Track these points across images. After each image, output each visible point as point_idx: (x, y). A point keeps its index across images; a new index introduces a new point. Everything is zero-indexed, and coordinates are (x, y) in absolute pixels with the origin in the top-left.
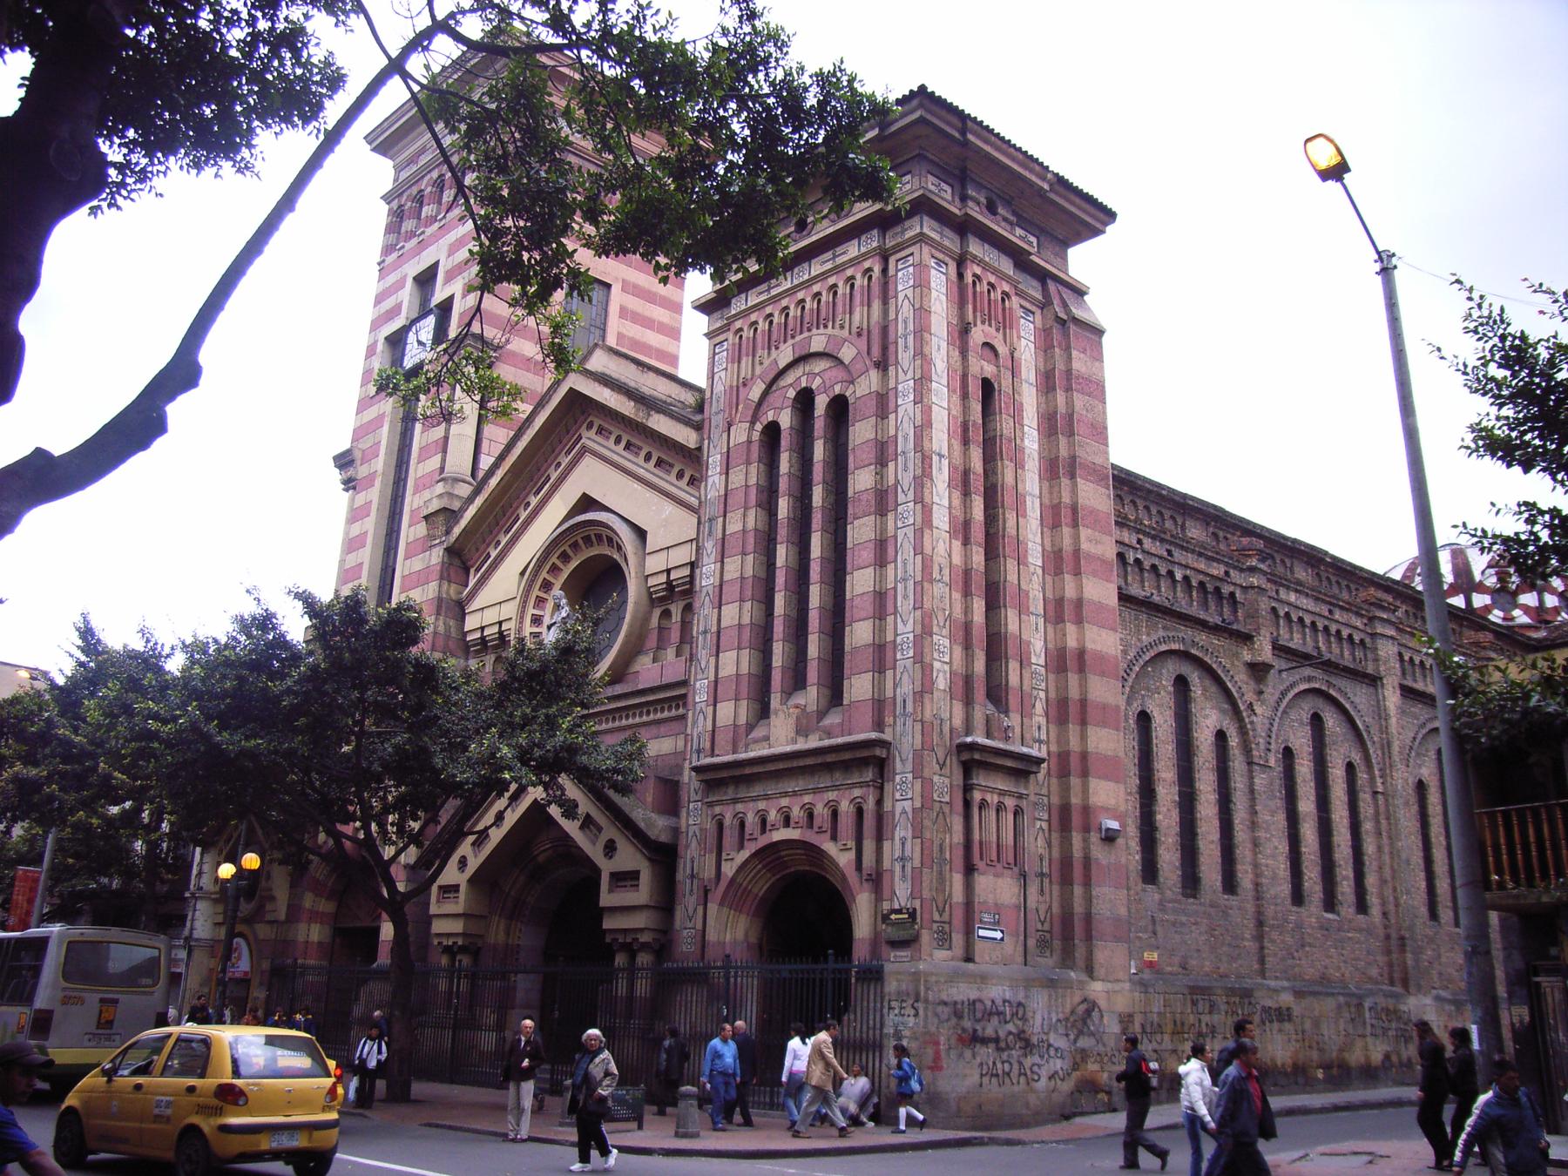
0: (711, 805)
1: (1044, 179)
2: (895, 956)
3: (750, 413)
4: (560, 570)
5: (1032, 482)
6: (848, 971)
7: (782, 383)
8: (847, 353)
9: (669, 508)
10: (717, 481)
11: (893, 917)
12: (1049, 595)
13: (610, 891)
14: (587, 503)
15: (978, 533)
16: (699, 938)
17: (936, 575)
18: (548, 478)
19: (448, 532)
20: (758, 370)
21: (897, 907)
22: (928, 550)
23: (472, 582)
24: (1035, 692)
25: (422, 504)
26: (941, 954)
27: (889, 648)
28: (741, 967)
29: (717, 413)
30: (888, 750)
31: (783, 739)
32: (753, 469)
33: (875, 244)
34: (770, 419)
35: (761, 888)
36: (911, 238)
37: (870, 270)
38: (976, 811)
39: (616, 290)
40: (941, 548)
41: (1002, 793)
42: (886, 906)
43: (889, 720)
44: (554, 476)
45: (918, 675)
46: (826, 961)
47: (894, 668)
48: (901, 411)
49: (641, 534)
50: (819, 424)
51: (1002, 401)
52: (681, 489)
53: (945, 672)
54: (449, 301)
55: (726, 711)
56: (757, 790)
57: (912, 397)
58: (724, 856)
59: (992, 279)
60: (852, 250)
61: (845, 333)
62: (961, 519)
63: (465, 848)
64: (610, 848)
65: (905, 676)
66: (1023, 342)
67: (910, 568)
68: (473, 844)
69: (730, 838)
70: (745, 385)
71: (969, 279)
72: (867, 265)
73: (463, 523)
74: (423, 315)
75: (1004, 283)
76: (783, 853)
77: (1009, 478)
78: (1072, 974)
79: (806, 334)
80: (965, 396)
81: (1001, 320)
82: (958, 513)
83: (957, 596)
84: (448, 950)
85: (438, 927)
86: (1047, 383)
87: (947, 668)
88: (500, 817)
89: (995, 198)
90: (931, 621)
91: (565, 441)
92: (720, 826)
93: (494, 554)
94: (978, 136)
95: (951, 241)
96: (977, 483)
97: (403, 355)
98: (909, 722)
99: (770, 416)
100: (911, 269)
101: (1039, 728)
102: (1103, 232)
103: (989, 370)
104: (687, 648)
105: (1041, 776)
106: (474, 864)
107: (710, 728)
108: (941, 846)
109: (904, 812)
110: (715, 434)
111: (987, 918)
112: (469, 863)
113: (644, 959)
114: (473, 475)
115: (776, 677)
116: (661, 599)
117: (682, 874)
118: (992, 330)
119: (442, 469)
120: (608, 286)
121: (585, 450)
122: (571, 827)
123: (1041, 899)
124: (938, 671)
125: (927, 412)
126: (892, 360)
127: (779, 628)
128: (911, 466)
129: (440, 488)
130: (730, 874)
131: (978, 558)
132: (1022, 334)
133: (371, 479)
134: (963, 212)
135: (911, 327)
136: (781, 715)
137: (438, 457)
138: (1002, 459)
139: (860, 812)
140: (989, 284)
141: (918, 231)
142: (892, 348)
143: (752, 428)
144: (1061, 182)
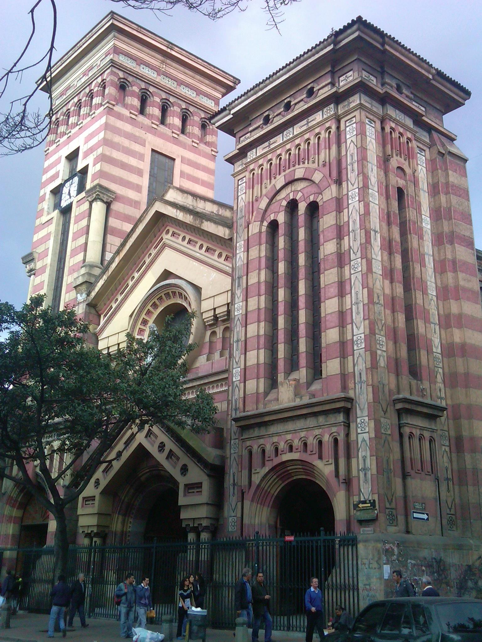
0: (244, 440)
1: (429, 72)
2: (363, 531)
3: (260, 216)
4: (152, 313)
5: (428, 247)
6: (333, 541)
7: (278, 197)
8: (317, 177)
9: (215, 274)
10: (242, 256)
11: (361, 505)
12: (441, 312)
13: (185, 495)
14: (166, 274)
15: (399, 276)
16: (240, 522)
17: (376, 300)
18: (145, 262)
19: (88, 295)
20: (264, 192)
21: (362, 499)
22: (371, 285)
23: (102, 322)
24: (436, 369)
25: (73, 280)
26: (392, 529)
27: (349, 343)
28: (264, 540)
29: (241, 218)
30: (352, 403)
31: (286, 400)
32: (263, 247)
33: (332, 113)
34: (272, 219)
35: (275, 491)
36: (354, 107)
37: (329, 128)
38: (406, 440)
39: (178, 162)
40: (378, 285)
41: (422, 429)
42: (356, 499)
43: (351, 385)
44: (148, 261)
45: (369, 358)
46: (319, 534)
47: (353, 355)
48: (351, 207)
49: (198, 289)
51: (408, 201)
52: (221, 263)
53: (384, 357)
54: (86, 168)
55: (251, 385)
56: (273, 429)
57: (357, 198)
58: (253, 471)
59: (401, 130)
60: (318, 117)
61: (316, 165)
62: (389, 268)
63: (99, 474)
64: (184, 470)
65: (360, 360)
66: (420, 167)
67: (360, 296)
68: (103, 471)
69: (257, 460)
70: (257, 200)
71: (388, 130)
72: (327, 125)
73: (97, 289)
74: (71, 178)
75: (408, 133)
76: (289, 468)
77: (415, 244)
78: (471, 541)
79: (292, 169)
80: (388, 197)
81: (407, 153)
82: (387, 264)
83: (388, 312)
84: (88, 535)
85: (82, 521)
86: (434, 190)
87: (385, 354)
88: (119, 454)
89: (401, 84)
90: (375, 327)
91: (121, 576)
92: (250, 453)
93: (114, 306)
94: (392, 47)
95: (377, 108)
96: (397, 247)
97: (61, 200)
98: (364, 386)
99: (272, 217)
100: (354, 125)
101: (440, 390)
102: (464, 104)
103: (401, 183)
104: (227, 353)
105: (443, 419)
106: (103, 483)
107: (242, 395)
108: (387, 461)
109: (364, 440)
110: (240, 229)
111: (418, 506)
112: (101, 483)
113: (204, 536)
114: (102, 263)
115: (281, 364)
116: (210, 325)
117: (229, 481)
118: (402, 160)
119: (84, 260)
120: (174, 160)
121: (165, 246)
122: (161, 458)
123: (448, 494)
124: (380, 356)
125: (367, 206)
126: (344, 177)
127: (281, 336)
128: (358, 237)
129: (83, 271)
130: (257, 482)
131: (399, 290)
132: (419, 162)
133: (43, 269)
134: (384, 91)
135: (355, 158)
136: (285, 386)
137: (82, 254)
138: (410, 233)
139: (336, 441)
140: (400, 133)
141: (358, 102)
142: (344, 172)
143: (261, 225)
144: (440, 74)
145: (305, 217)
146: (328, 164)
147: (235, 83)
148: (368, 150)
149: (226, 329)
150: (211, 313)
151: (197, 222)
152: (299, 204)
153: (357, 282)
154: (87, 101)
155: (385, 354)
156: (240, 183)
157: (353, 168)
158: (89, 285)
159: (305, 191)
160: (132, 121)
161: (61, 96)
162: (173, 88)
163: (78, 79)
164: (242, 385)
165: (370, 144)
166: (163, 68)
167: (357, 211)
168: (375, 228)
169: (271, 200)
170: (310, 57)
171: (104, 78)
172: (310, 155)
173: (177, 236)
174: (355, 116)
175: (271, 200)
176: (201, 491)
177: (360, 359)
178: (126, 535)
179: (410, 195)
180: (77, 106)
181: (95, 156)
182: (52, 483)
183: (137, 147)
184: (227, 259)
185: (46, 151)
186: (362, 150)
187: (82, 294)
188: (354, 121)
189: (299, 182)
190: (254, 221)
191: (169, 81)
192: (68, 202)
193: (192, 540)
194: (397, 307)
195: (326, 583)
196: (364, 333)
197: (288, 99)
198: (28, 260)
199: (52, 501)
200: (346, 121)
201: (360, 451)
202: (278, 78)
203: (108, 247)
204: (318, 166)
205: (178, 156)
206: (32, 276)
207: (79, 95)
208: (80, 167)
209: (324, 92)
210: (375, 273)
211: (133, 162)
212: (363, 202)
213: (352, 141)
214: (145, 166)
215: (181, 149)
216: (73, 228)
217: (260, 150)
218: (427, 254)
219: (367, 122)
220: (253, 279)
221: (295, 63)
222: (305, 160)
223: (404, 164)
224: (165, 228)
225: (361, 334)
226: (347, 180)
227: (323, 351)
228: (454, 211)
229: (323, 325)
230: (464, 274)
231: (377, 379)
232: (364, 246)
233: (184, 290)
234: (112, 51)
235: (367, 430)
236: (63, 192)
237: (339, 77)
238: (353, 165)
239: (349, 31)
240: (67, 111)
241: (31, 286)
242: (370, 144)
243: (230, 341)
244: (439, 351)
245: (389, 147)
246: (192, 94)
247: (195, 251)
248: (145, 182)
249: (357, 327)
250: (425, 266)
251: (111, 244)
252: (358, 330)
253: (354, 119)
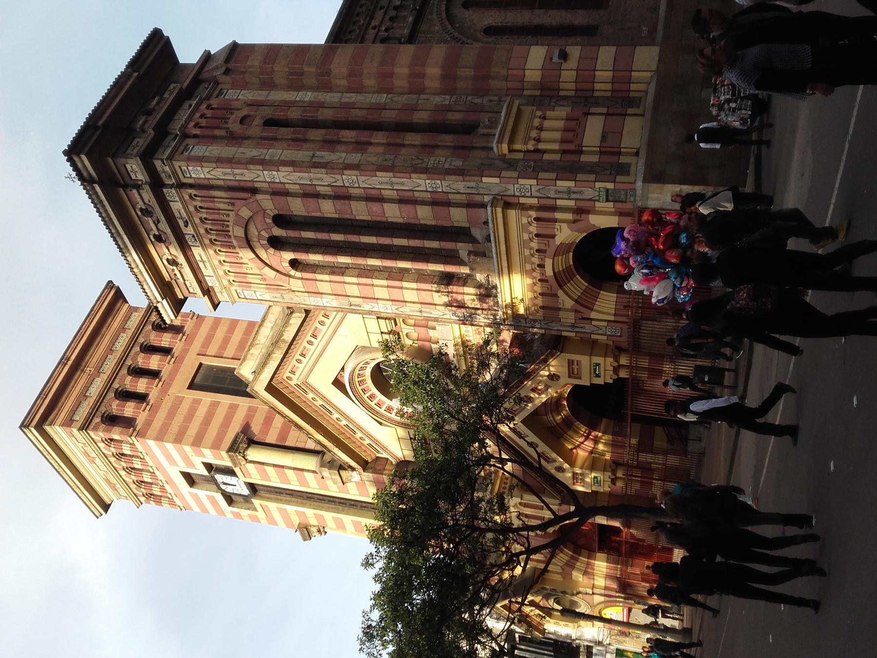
5: (333, 98)
8: (245, 213)
10: (327, 300)
11: (597, 373)
14: (338, 383)
15: (364, 136)
17: (390, 163)
19: (353, 469)
23: (385, 455)
37: (190, 196)
40: (373, 159)
50: (292, 234)
51: (279, 115)
53: (452, 161)
57: (275, 173)
59: (198, 115)
60: (176, 207)
70: (265, 280)
71: (197, 131)
72: (187, 197)
80: (275, 139)
84: (613, 481)
86: (268, 84)
93: (368, 441)
96: (331, 134)
100: (190, 168)
103: (258, 121)
104: (431, 323)
109: (539, 191)
118: (233, 117)
120: (201, 364)
124: (450, 165)
126: (249, 185)
131: (380, 137)
132: (235, 97)
133: (318, 517)
135: (229, 170)
138: (317, 117)
142: (242, 184)
145: (290, 229)
146: (232, 201)
147: (112, 288)
148: (220, 156)
151: (282, 345)
152: (274, 235)
153: (368, 182)
154: (127, 461)
155: (449, 160)
156: (243, 297)
157: (239, 175)
159: (260, 227)
160: (154, 410)
161: (116, 490)
162: (116, 360)
163: (98, 469)
165: (213, 152)
166: (90, 371)
167: (288, 174)
168: (309, 156)
169: (266, 264)
170: (106, 211)
172: (220, 219)
173: (295, 368)
174: (180, 167)
175: (266, 264)
176: (577, 361)
177: (452, 186)
178: (617, 442)
179: (273, 112)
180: (130, 472)
181: (193, 454)
182: (557, 519)
184: (326, 316)
185: (181, 510)
186: (220, 161)
189: (248, 232)
191: (107, 364)
192: (244, 487)
193: (627, 362)
194: (399, 141)
196: (425, 180)
197: (152, 237)
199: (576, 519)
200: (185, 177)
201: (549, 195)
203: (300, 445)
204: (232, 211)
205: (197, 358)
206: (326, 530)
207: (118, 470)
208: (205, 472)
209: (148, 195)
210: (360, 161)
211: (201, 412)
212: (280, 168)
213: (208, 172)
214: (207, 398)
215: (189, 355)
216: (275, 481)
218: (341, 99)
219: (187, 153)
221: (111, 228)
222: (224, 224)
223: (237, 115)
224: (285, 380)
225: (425, 183)
226: (252, 181)
227: (440, 223)
228: (294, 64)
229: (412, 221)
230: (365, 60)
231: (475, 170)
232: (329, 171)
234: (68, 429)
235: (529, 187)
236: (232, 492)
237: (132, 179)
238: (236, 174)
239: (80, 165)
240: (135, 483)
242: (213, 152)
243: (419, 320)
244: (448, 97)
245: (218, 133)
247: (313, 351)
248: (226, 400)
250: (354, 103)
251: (297, 441)
252: (421, 185)
253: (183, 168)
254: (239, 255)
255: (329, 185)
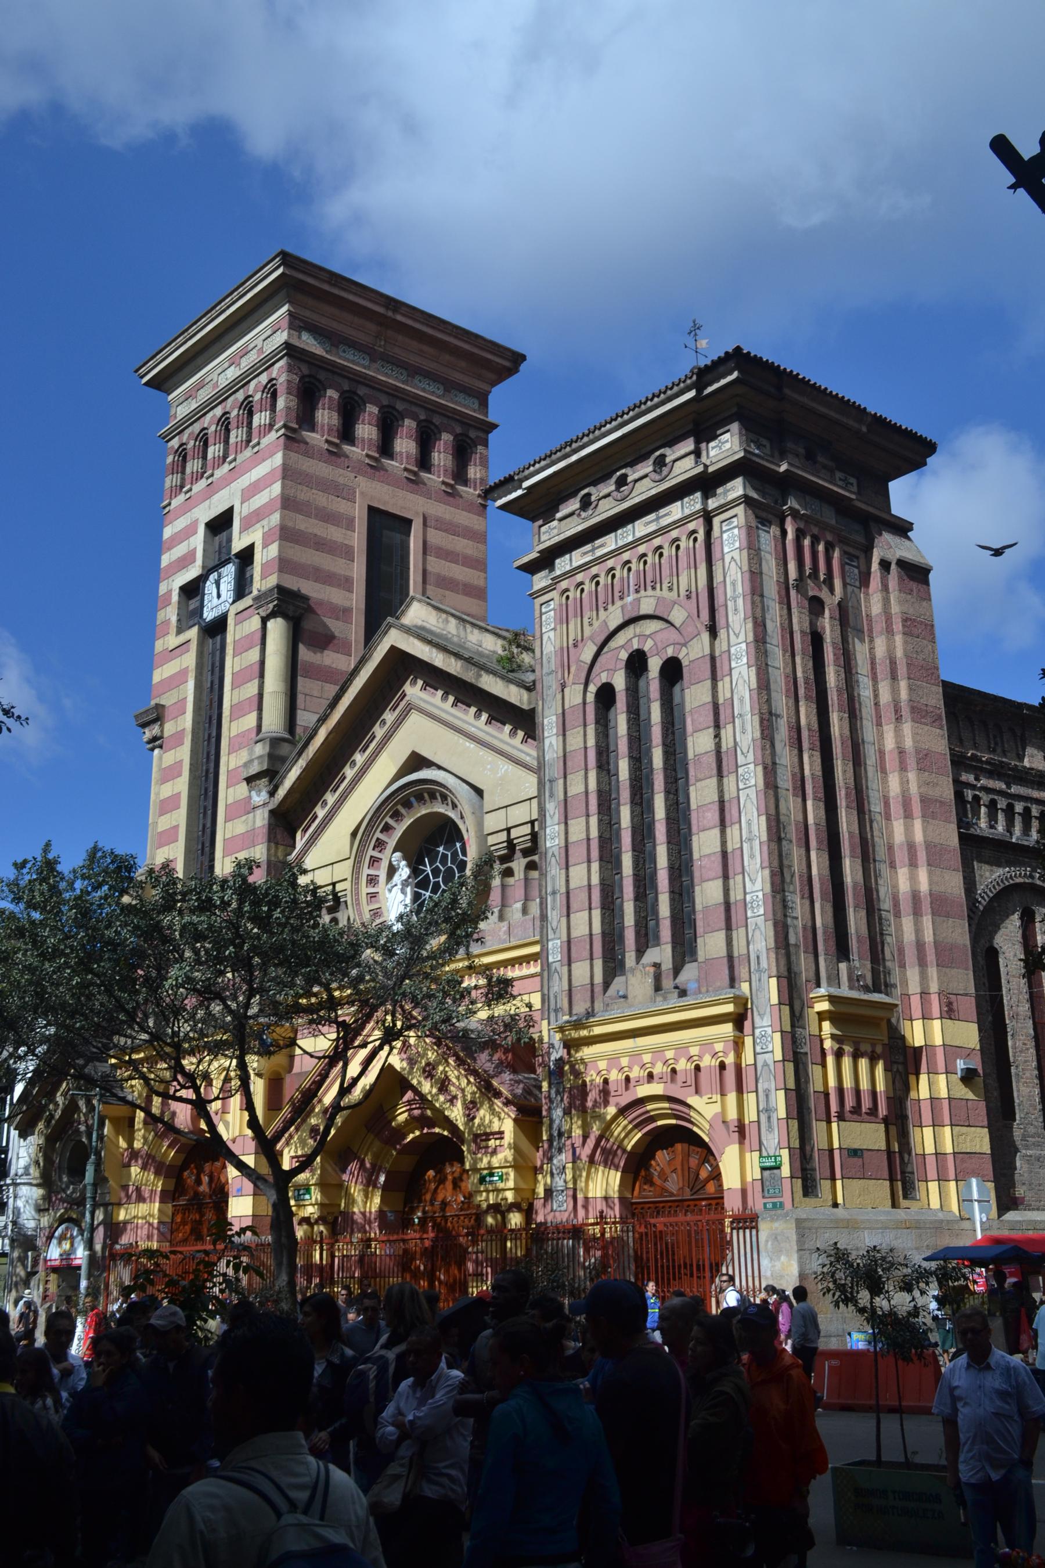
3: (584, 675)
7: (613, 644)
8: (678, 616)
9: (505, 767)
10: (554, 742)
14: (417, 761)
23: (300, 843)
29: (549, 674)
34: (604, 681)
37: (694, 532)
48: (735, 674)
54: (250, 549)
57: (745, 660)
60: (675, 511)
67: (755, 828)
70: (575, 646)
72: (691, 526)
99: (604, 678)
104: (534, 908)
109: (766, 1064)
121: (409, 708)
133: (179, 736)
135: (740, 590)
136: (638, 974)
146: (694, 595)
149: (531, 866)
150: (503, 836)
151: (471, 674)
152: (649, 660)
153: (749, 805)
156: (544, 610)
157: (735, 606)
158: (271, 774)
164: (566, 968)
171: (274, 376)
174: (736, 516)
177: (757, 933)
181: (266, 529)
183: (341, 506)
187: (260, 791)
188: (735, 524)
190: (574, 683)
195: (713, 1287)
198: (146, 719)
202: (604, 435)
206: (157, 751)
207: (223, 404)
209: (684, 469)
214: (358, 539)
217: (578, 557)
220: (576, 787)
227: (699, 917)
233: (451, 791)
235: (770, 1049)
241: (155, 769)
246: (436, 390)
249: (751, 880)
252: (754, 884)
254: (610, 606)
255: (736, 743)
